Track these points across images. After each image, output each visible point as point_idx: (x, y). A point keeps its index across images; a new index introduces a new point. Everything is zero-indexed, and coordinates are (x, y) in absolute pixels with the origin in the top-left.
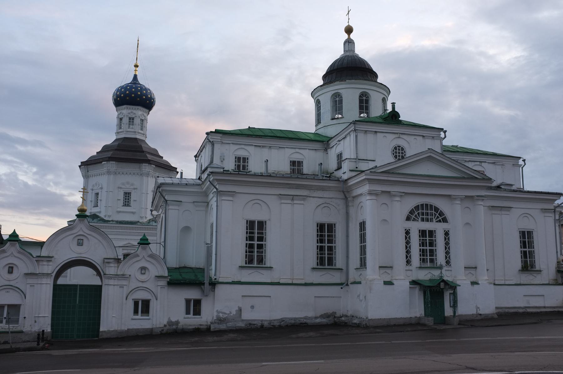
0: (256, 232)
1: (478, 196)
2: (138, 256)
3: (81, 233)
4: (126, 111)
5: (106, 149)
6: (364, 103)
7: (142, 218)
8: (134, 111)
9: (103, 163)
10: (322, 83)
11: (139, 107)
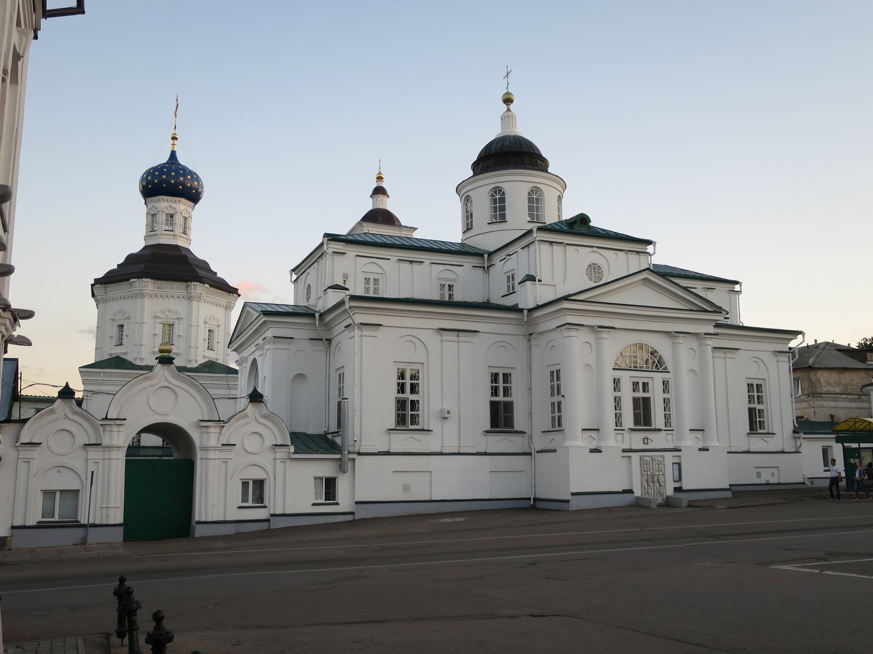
0: (408, 384)
1: (599, 327)
2: (247, 416)
3: (166, 384)
4: (164, 204)
5: (131, 258)
6: (535, 200)
7: (190, 361)
8: (174, 205)
9: (132, 280)
10: (471, 174)
11: (183, 200)
